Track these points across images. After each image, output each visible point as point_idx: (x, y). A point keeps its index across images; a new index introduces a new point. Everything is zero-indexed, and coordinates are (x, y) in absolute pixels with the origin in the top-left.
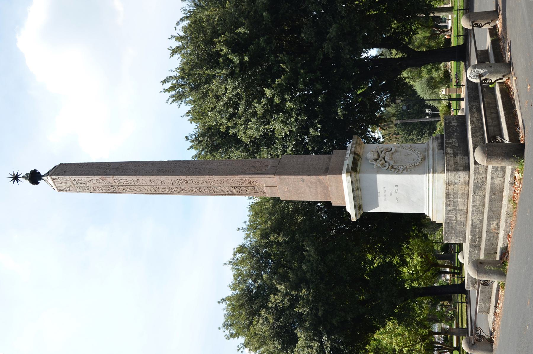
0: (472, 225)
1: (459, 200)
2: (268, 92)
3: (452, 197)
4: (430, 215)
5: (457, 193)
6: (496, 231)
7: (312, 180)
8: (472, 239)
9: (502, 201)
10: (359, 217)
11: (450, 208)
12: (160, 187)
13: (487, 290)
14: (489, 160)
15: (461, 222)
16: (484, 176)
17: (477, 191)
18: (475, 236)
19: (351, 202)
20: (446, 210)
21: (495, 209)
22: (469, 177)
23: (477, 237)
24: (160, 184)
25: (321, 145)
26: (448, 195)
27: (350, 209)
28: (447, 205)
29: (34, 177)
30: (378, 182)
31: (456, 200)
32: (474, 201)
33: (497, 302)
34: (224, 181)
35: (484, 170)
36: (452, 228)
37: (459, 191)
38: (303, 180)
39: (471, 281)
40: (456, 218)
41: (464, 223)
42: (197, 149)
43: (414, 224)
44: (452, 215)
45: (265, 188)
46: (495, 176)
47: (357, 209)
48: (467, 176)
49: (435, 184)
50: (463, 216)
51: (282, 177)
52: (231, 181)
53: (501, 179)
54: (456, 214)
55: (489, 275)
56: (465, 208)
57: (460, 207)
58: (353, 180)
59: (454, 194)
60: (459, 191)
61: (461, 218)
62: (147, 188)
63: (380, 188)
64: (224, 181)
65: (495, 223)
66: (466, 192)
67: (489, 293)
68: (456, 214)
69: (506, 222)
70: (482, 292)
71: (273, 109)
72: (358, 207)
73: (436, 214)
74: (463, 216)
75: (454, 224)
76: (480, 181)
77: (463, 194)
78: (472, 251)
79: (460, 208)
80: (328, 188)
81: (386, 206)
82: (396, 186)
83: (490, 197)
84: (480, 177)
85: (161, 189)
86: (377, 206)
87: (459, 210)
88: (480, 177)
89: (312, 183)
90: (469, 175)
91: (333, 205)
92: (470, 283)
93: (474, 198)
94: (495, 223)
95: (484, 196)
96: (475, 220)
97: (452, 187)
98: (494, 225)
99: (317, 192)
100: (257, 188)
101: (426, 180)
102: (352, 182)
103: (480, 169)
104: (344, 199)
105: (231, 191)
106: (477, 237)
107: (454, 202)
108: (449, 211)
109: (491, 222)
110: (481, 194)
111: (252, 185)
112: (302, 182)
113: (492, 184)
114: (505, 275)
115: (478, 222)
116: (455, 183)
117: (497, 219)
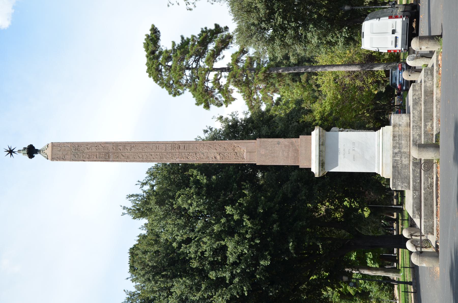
1: (403, 142)
2: (229, 209)
3: (397, 138)
4: (380, 174)
6: (431, 133)
7: (286, 143)
10: (321, 175)
11: (396, 150)
12: (152, 154)
13: (429, 203)
14: (421, 41)
15: (405, 165)
16: (420, 92)
17: (415, 107)
19: (316, 156)
21: (429, 110)
24: (154, 151)
25: (268, 287)
26: (394, 137)
27: (315, 169)
28: (394, 147)
29: (31, 151)
30: (339, 140)
32: (413, 117)
33: (437, 205)
34: (212, 146)
35: (419, 87)
36: (398, 173)
37: (403, 133)
38: (279, 143)
39: (416, 207)
40: (401, 161)
41: (407, 167)
42: (202, 103)
43: (365, 184)
45: (245, 153)
46: (426, 79)
47: (321, 164)
48: (408, 118)
49: (385, 137)
50: (407, 159)
51: (263, 139)
52: (218, 146)
53: (431, 82)
54: (401, 158)
55: (427, 148)
56: (408, 151)
57: (404, 150)
58: (321, 134)
59: (399, 136)
60: (403, 133)
62: (140, 156)
63: (341, 146)
64: (212, 146)
65: (430, 124)
66: (408, 134)
68: (401, 158)
69: (437, 108)
70: (425, 205)
71: (231, 230)
72: (322, 164)
73: (384, 171)
74: (407, 159)
75: (400, 168)
76: (417, 98)
77: (406, 135)
78: (415, 169)
80: (298, 151)
81: (345, 165)
82: (354, 143)
83: (425, 99)
84: (417, 93)
85: (153, 156)
86: (337, 165)
88: (417, 93)
90: (410, 117)
91: (300, 167)
92: (415, 209)
93: (413, 114)
94: (430, 124)
95: (421, 111)
97: (397, 129)
98: (429, 126)
99: (288, 155)
100: (238, 154)
103: (416, 86)
104: (310, 160)
105: (215, 158)
108: (396, 153)
109: (427, 123)
110: (418, 109)
111: (236, 151)
112: (277, 145)
113: (425, 86)
114: (439, 147)
115: (418, 137)
116: (400, 125)
117: (431, 120)
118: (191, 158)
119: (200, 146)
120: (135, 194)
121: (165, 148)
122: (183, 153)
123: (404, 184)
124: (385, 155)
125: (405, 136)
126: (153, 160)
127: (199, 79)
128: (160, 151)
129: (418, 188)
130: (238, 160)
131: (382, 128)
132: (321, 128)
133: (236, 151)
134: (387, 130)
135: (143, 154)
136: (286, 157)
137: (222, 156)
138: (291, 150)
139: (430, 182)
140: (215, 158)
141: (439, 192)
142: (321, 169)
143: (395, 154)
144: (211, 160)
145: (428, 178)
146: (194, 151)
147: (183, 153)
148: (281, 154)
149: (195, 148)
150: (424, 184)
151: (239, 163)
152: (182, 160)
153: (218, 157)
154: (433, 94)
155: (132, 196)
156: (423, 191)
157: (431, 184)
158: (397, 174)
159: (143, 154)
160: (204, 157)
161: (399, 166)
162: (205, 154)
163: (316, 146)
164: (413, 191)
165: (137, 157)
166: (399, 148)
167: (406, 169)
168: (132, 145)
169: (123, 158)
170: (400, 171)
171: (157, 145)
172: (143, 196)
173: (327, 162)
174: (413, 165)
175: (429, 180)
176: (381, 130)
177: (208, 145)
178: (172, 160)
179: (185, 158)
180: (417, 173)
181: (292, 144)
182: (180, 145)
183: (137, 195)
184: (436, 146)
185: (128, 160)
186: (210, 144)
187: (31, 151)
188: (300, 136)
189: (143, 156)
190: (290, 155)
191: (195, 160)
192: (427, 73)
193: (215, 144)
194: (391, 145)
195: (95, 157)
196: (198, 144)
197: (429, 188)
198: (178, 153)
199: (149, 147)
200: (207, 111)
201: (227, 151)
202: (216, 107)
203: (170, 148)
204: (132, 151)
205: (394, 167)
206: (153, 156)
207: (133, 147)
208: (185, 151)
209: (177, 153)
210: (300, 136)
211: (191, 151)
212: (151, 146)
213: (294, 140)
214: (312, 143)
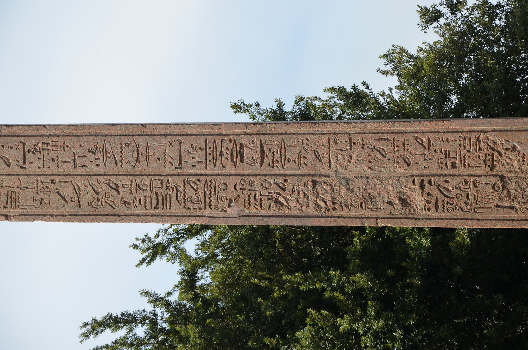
12: (121, 181)
24: (126, 168)
34: (387, 148)
62: (68, 192)
64: (387, 148)
85: (125, 194)
100: (512, 185)
105: (404, 202)
111: (500, 169)
118: (293, 204)
119: (335, 149)
120: (117, 312)
121: (175, 155)
122: (257, 181)
126: (123, 210)
128: (154, 167)
130: (513, 215)
133: (500, 169)
135: (81, 182)
137: (435, 192)
140: (404, 202)
144: (384, 211)
146: (304, 170)
147: (257, 181)
149: (311, 156)
151: (516, 226)
152: (253, 211)
153: (418, 199)
155: (112, 322)
159: (81, 182)
160: (352, 200)
162: (358, 185)
165: (55, 197)
168: (30, 143)
171: (142, 142)
172: (153, 323)
177: (370, 140)
178: (207, 212)
179: (265, 203)
182: (245, 140)
183: (128, 320)
185: (11, 212)
186: (379, 136)
189: (77, 191)
191: (312, 211)
193: (401, 138)
196: (324, 140)
198: (234, 180)
199: (104, 151)
200: (386, 49)
201: (461, 169)
202: (406, 48)
203: (199, 155)
204: (30, 168)
206: (125, 194)
207: (35, 150)
208: (267, 170)
209: (232, 181)
211: (291, 169)
212: (113, 146)
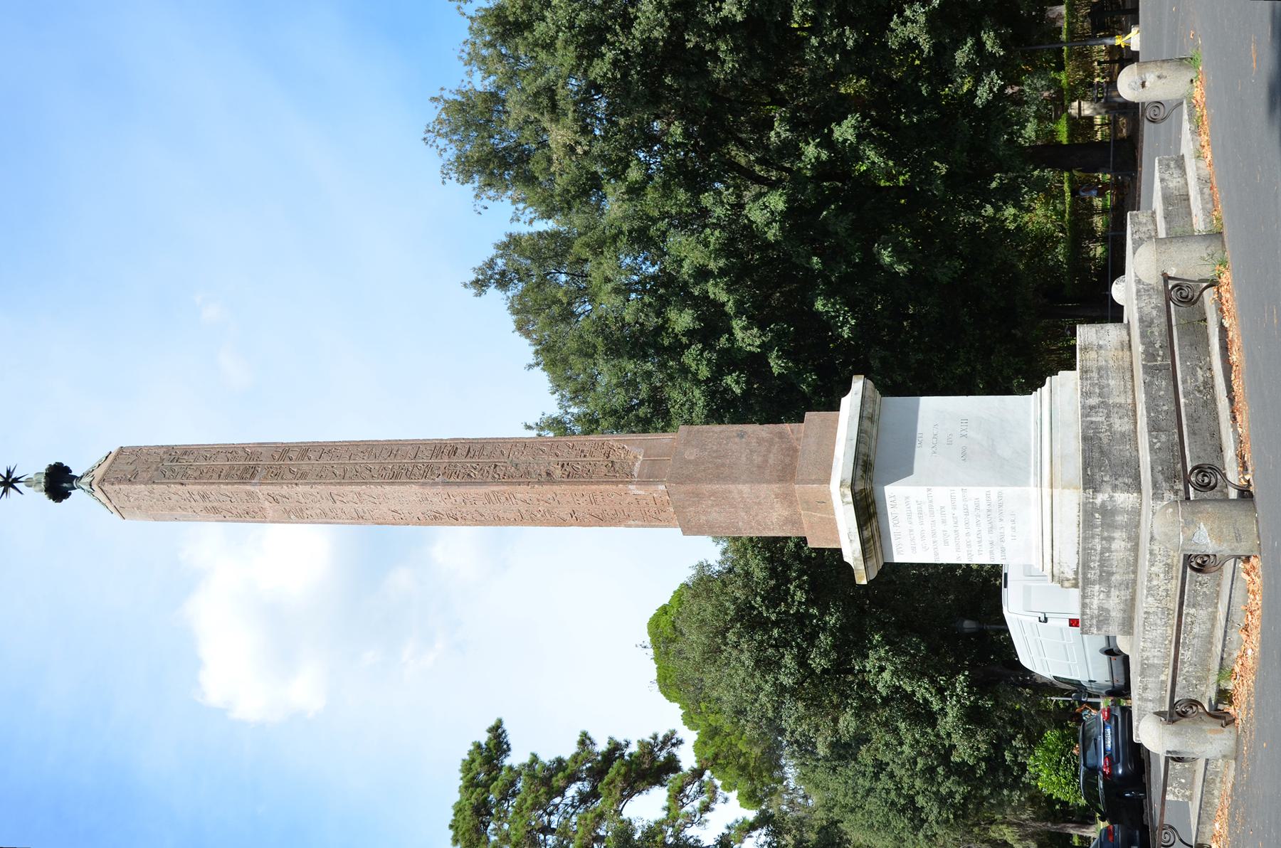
0: (1141, 320)
1: (1112, 382)
3: (1095, 375)
5: (1107, 369)
8: (1146, 352)
9: (1190, 214)
11: (1093, 401)
13: (1205, 426)
15: (1123, 435)
18: (1152, 344)
20: (1083, 407)
22: (1129, 334)
23: (1157, 346)
28: (1086, 395)
29: (58, 482)
31: (1104, 382)
36: (1102, 452)
37: (1111, 363)
39: (1162, 472)
40: (1110, 425)
41: (1132, 437)
44: (1098, 419)
46: (1166, 176)
47: (860, 462)
48: (1124, 333)
50: (1126, 419)
54: (1108, 416)
56: (1129, 401)
58: (867, 394)
59: (1099, 369)
60: (1111, 363)
61: (1121, 425)
66: (1127, 364)
67: (1212, 435)
68: (1108, 416)
70: (1193, 433)
74: (1126, 419)
75: (1105, 441)
77: (1120, 369)
79: (1118, 400)
82: (965, 421)
87: (1115, 405)
89: (760, 441)
92: (1160, 477)
96: (1147, 310)
101: (1036, 430)
102: (863, 397)
104: (834, 530)
105: (548, 474)
106: (1157, 346)
107: (1101, 387)
108: (1092, 408)
111: (612, 458)
112: (737, 440)
113: (1165, 190)
115: (1154, 313)
116: (1100, 347)
123: (1120, 480)
124: (1057, 436)
125: (1118, 368)
127: (586, 261)
129: (1167, 421)
131: (1048, 379)
132: (870, 383)
133: (612, 458)
134: (1063, 388)
136: (759, 467)
138: (775, 449)
139: (1201, 379)
141: (1234, 357)
142: (860, 472)
143: (1088, 411)
145: (1194, 369)
148: (744, 458)
150: (1184, 382)
154: (1187, 199)
156: (1182, 400)
157: (1205, 383)
158: (1096, 455)
161: (1102, 435)
163: (851, 418)
164: (1150, 432)
166: (1100, 395)
167: (1124, 443)
169: (291, 476)
170: (1106, 448)
173: (879, 462)
174: (1145, 373)
175: (1200, 372)
176: (1046, 388)
180: (1160, 389)
181: (781, 435)
184: (1219, 716)
187: (58, 482)
188: (808, 415)
190: (771, 461)
192: (1168, 166)
194: (1076, 412)
195: (215, 476)
197: (1200, 391)
205: (1085, 439)
210: (808, 415)
213: (787, 427)
214: (839, 527)
